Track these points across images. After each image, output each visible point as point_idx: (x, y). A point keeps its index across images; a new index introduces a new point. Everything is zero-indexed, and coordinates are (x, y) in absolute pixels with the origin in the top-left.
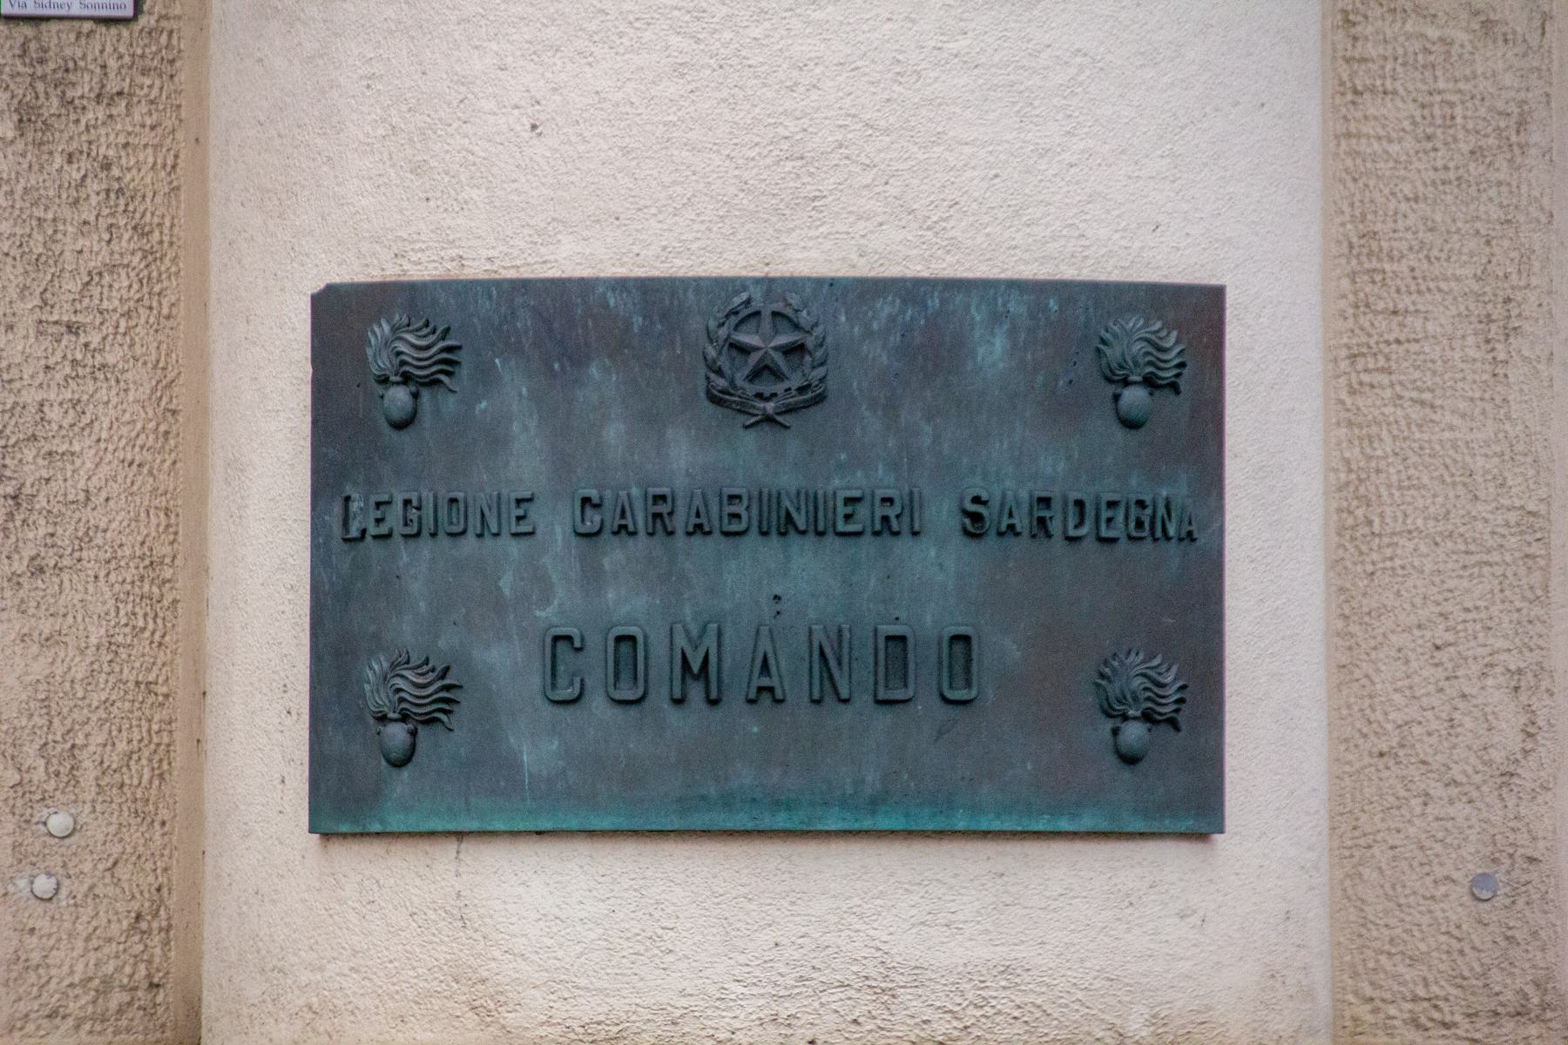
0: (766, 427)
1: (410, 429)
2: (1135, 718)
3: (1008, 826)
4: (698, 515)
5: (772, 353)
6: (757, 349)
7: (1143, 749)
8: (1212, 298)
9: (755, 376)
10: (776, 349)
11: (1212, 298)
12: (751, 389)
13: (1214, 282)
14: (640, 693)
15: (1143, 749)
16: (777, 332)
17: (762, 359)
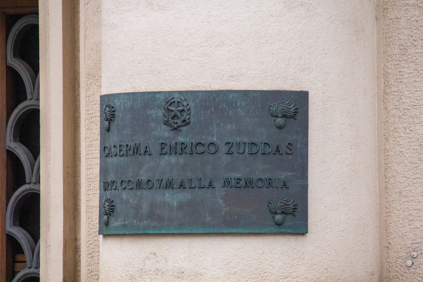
0: (176, 130)
1: (197, 142)
2: (280, 117)
3: (245, 231)
4: (146, 148)
5: (177, 112)
6: (174, 111)
7: (284, 212)
8: (302, 97)
9: (173, 118)
10: (178, 111)
11: (302, 97)
12: (172, 121)
13: (304, 89)
14: (290, 153)
15: (284, 212)
16: (179, 107)
17: (175, 113)
